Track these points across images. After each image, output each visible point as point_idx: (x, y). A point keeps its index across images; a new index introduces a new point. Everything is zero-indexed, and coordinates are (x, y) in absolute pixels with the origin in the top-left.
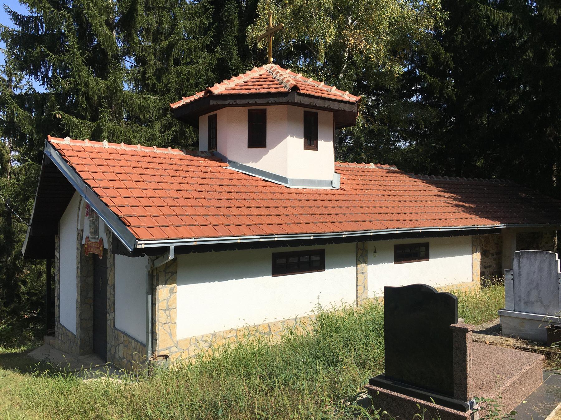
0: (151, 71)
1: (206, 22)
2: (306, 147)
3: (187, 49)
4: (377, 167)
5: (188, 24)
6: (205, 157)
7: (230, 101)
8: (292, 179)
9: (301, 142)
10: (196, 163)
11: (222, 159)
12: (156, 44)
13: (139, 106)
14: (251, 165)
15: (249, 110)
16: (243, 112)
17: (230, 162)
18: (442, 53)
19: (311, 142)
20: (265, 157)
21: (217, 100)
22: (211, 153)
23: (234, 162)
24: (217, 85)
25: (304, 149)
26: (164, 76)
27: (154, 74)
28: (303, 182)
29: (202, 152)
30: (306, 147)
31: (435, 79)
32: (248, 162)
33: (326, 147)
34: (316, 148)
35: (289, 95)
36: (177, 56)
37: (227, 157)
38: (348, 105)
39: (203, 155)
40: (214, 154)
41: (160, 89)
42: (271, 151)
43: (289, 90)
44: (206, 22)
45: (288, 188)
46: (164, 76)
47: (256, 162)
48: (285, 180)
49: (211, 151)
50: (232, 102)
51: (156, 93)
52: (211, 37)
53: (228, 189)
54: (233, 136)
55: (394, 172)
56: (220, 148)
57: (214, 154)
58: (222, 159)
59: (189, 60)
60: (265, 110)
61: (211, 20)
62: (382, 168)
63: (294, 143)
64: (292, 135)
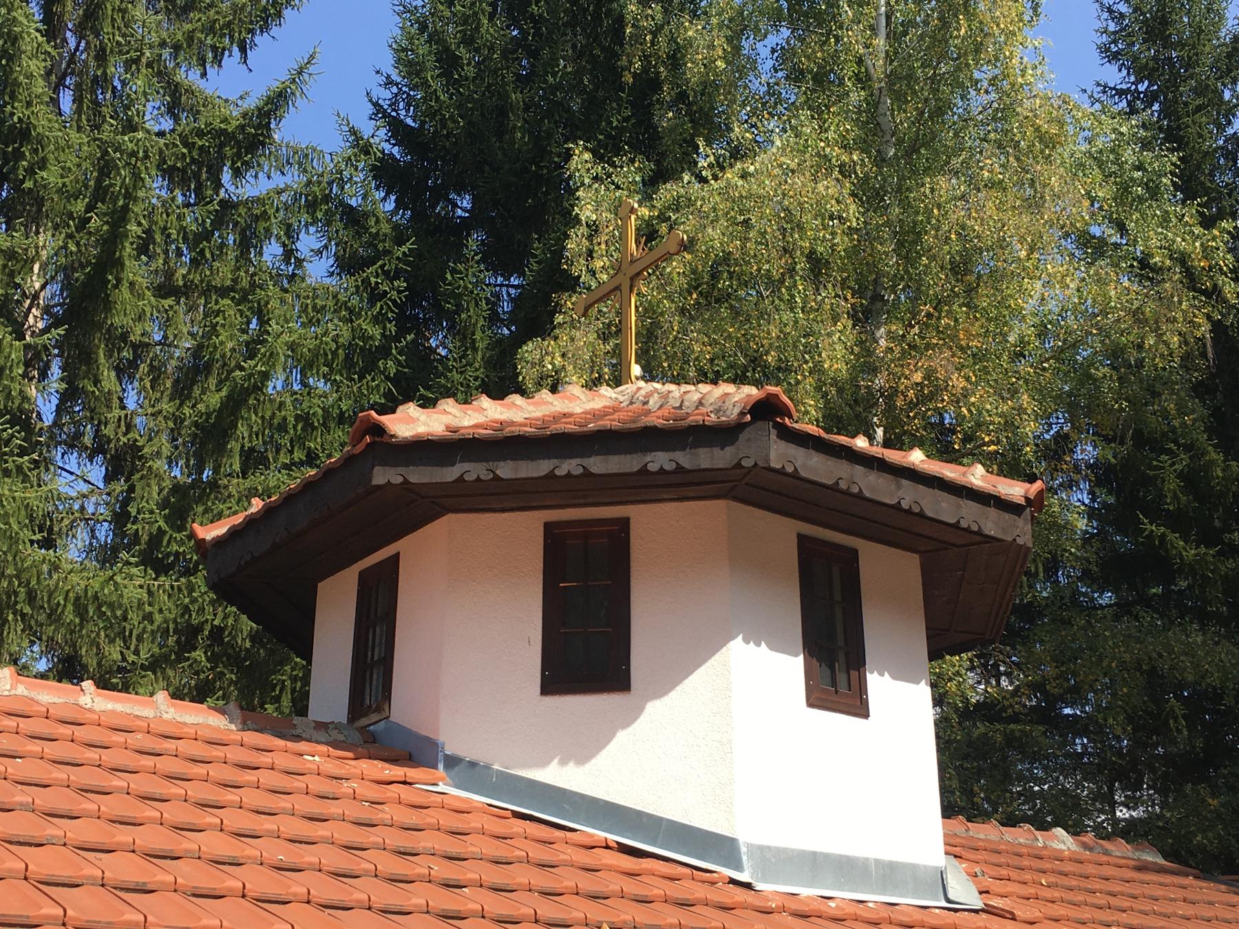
0: (150, 497)
1: (375, 332)
2: (817, 699)
3: (297, 418)
4: (1085, 846)
5: (308, 338)
6: (335, 745)
7: (466, 466)
8: (762, 848)
9: (788, 670)
10: (282, 761)
11: (413, 751)
12: (181, 405)
13: (77, 598)
14: (555, 774)
15: (548, 527)
16: (523, 532)
17: (452, 762)
18: (1212, 462)
19: (837, 678)
20: (622, 736)
21: (407, 464)
22: (363, 730)
23: (473, 764)
24: (411, 409)
25: (811, 704)
26: (200, 509)
27: (164, 504)
28: (815, 864)
29: (321, 726)
30: (817, 699)
31: (1203, 550)
32: (544, 763)
33: (903, 707)
34: (858, 707)
35: (743, 437)
36: (258, 443)
37: (442, 738)
38: (993, 512)
39: (322, 736)
40: (373, 724)
41: (177, 554)
42: (654, 708)
43: (742, 414)
44: (375, 332)
45: (748, 886)
46: (200, 509)
47: (582, 760)
48: (725, 848)
49: (364, 722)
50: (474, 470)
51: (161, 568)
52: (388, 378)
53: (442, 870)
54: (470, 630)
55: (1160, 870)
56: (407, 705)
57: (373, 724)
58: (413, 751)
59: (299, 455)
60: (625, 523)
61: (392, 328)
62: (1106, 853)
63: (759, 674)
64: (754, 637)
